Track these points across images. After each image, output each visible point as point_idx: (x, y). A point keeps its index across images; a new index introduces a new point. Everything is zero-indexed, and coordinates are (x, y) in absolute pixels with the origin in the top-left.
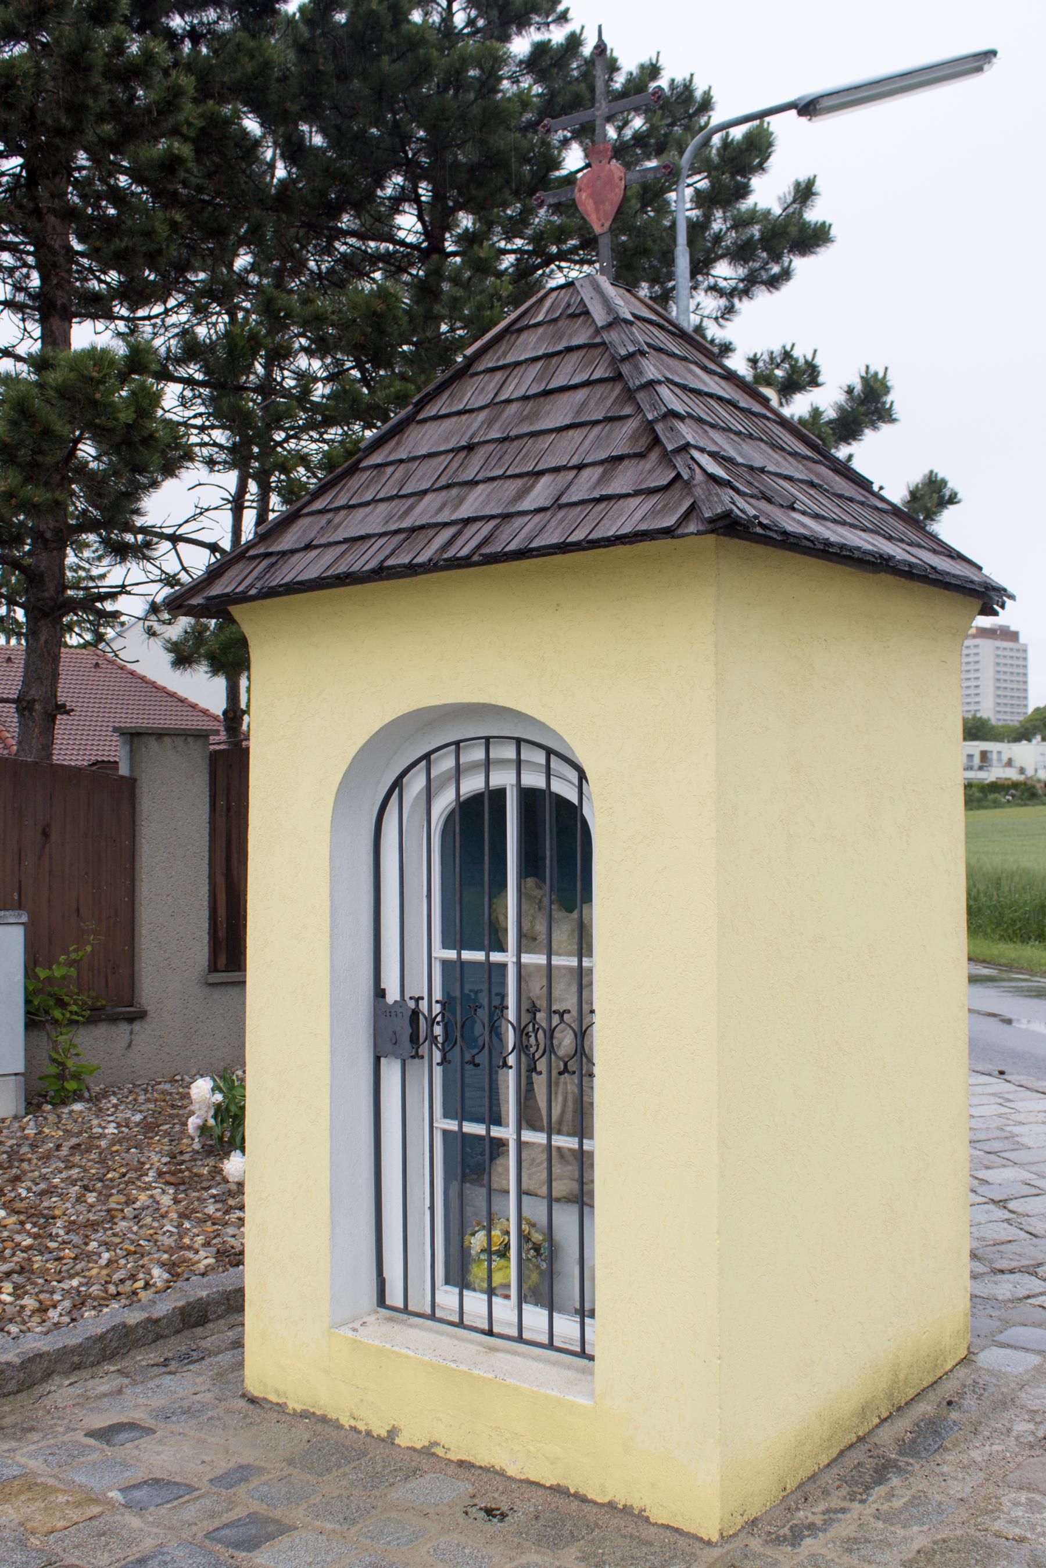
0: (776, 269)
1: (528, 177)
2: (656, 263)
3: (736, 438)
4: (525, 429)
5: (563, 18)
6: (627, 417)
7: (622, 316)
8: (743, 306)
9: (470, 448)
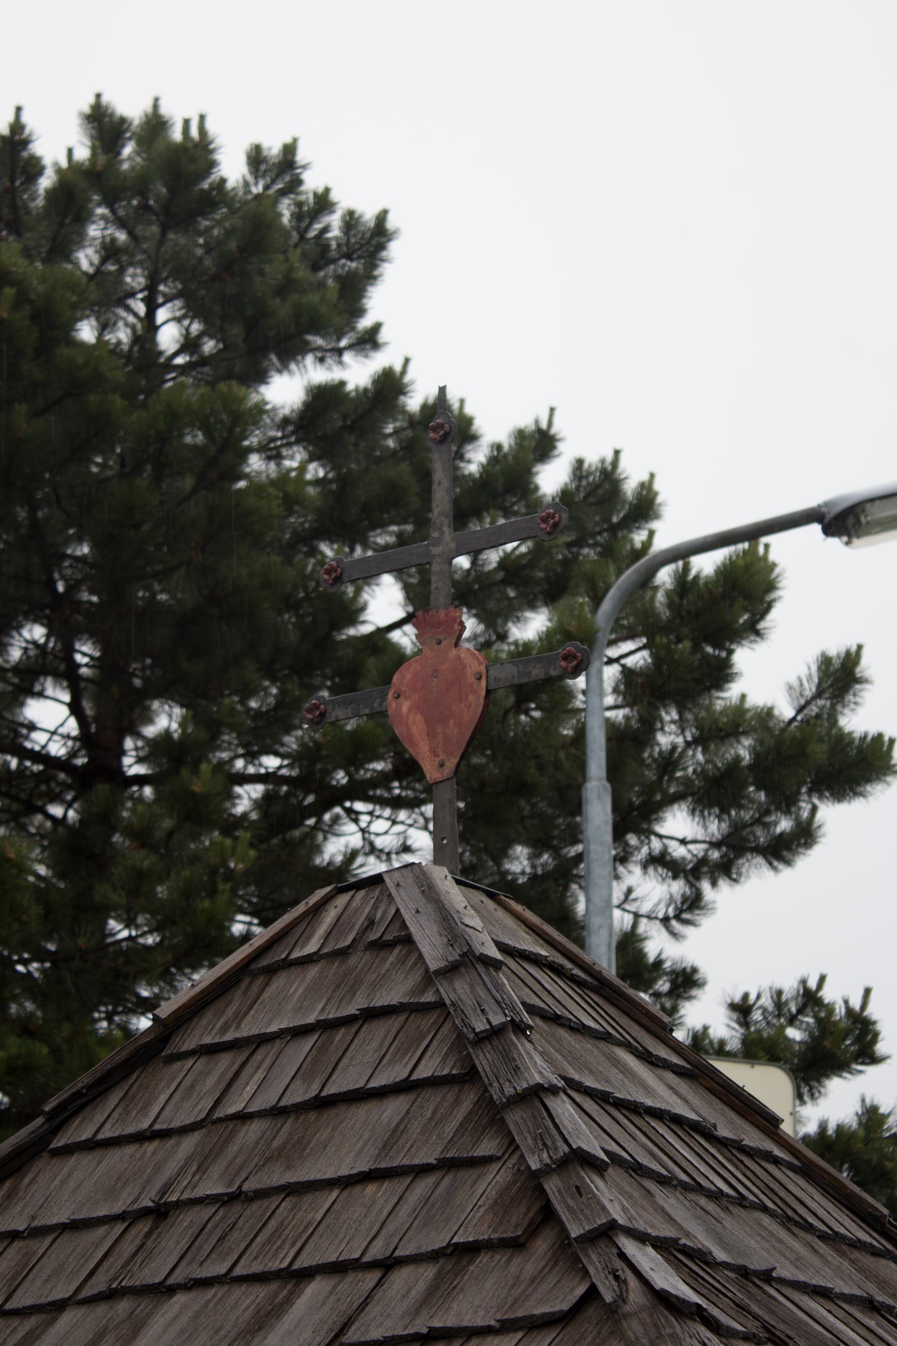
0: (784, 825)
1: (293, 636)
2: (543, 806)
3: (711, 1207)
4: (277, 1177)
5: (370, 341)
6: (487, 1160)
7: (479, 949)
8: (720, 895)
9: (160, 1213)
